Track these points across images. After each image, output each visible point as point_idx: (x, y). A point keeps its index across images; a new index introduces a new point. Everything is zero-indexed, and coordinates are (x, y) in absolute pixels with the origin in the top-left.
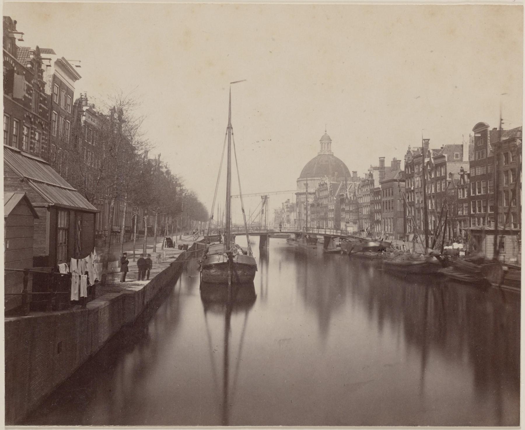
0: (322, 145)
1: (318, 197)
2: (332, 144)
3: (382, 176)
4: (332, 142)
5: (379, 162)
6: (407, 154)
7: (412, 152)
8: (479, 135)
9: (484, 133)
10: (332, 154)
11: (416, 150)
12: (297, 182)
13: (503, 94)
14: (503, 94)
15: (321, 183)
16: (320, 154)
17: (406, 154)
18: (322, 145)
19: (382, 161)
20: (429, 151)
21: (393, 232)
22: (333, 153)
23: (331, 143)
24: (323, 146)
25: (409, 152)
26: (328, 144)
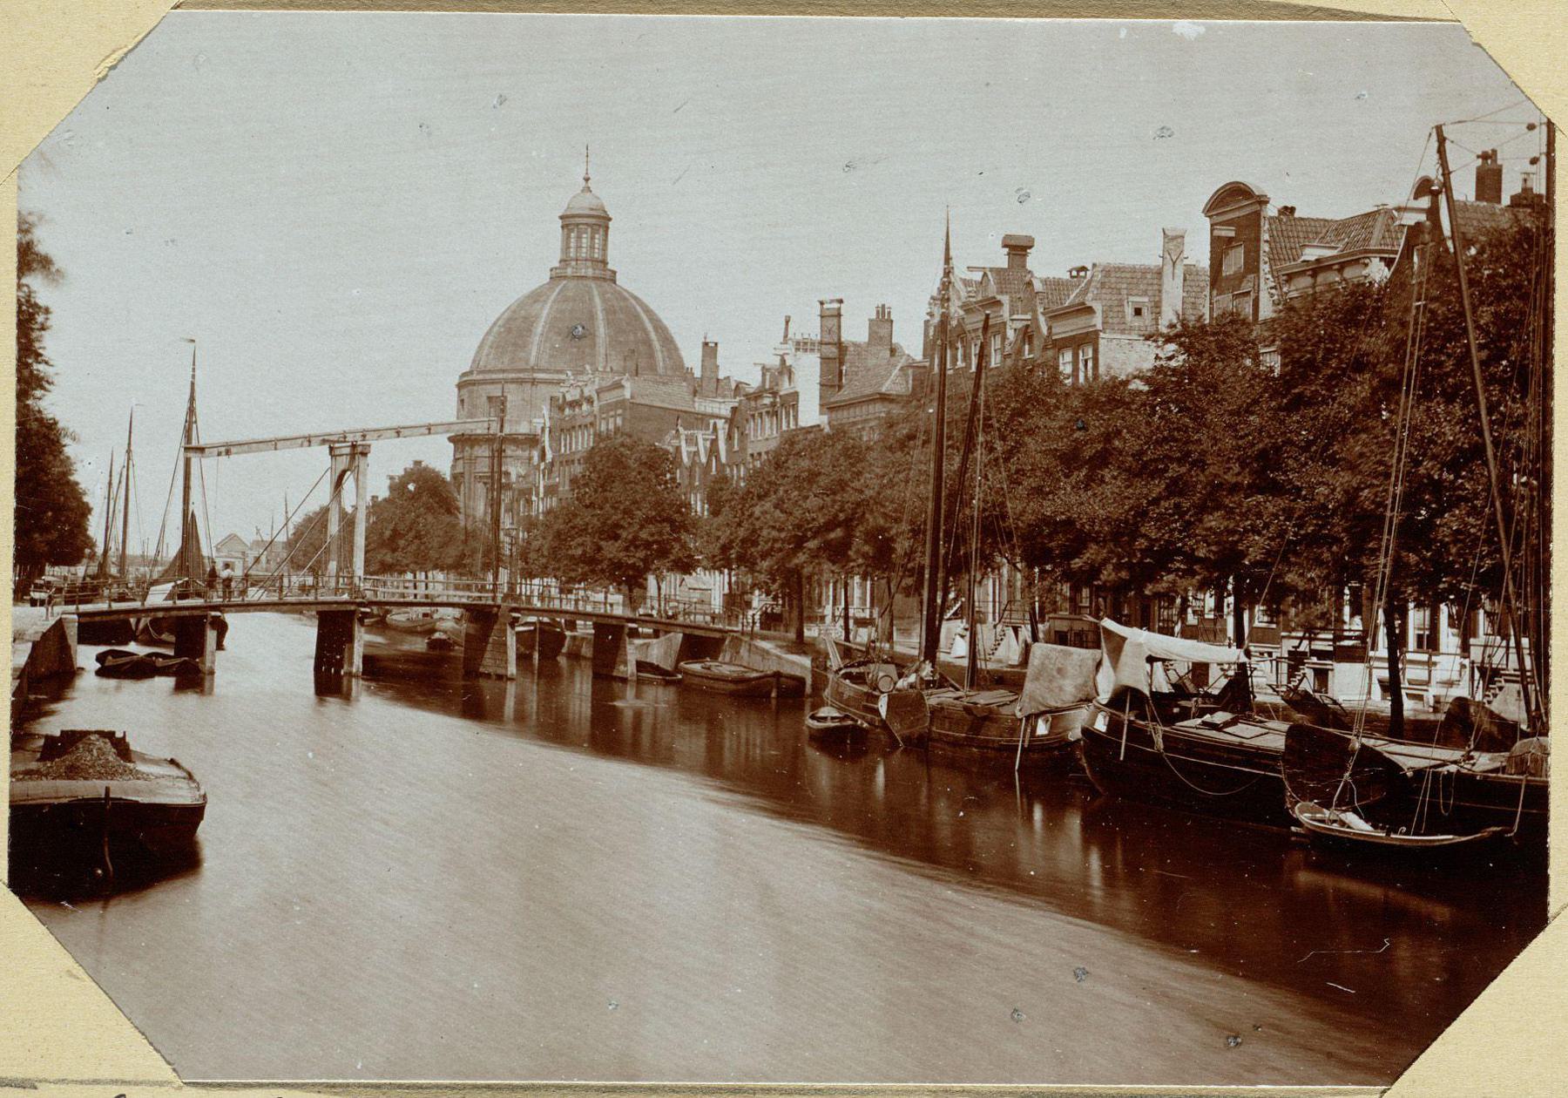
3: (833, 379)
12: (460, 386)
19: (831, 318)
22: (614, 273)
23: (607, 228)
26: (594, 233)
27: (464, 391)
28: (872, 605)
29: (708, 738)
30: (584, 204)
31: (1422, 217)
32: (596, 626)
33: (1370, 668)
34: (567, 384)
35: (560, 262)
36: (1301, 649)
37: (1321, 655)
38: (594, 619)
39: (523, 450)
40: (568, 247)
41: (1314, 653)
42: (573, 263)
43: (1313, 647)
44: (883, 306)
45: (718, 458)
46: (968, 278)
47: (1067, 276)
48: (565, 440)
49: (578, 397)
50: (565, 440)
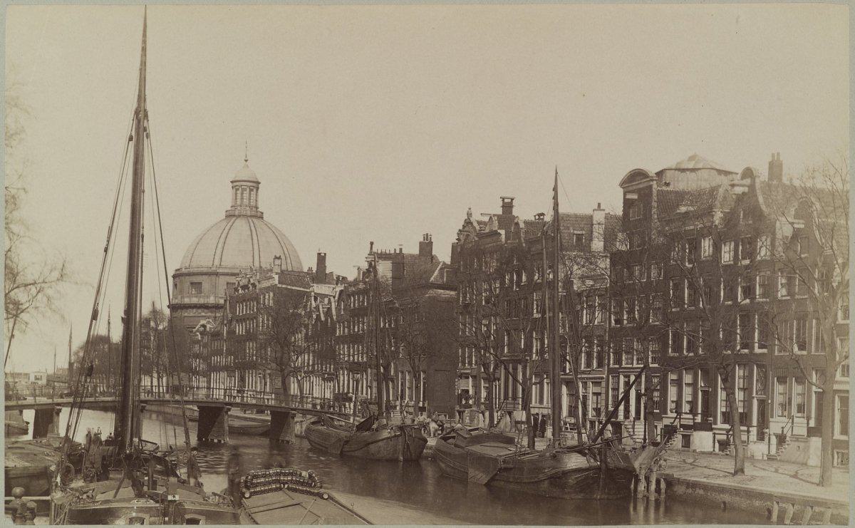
0: (236, 194)
1: (230, 316)
2: (260, 190)
4: (260, 185)
5: (4, 426)
6: (464, 226)
7: (475, 224)
8: (635, 197)
9: (645, 194)
10: (259, 214)
11: (486, 219)
13: (153, 303)
14: (153, 303)
15: (241, 284)
16: (232, 213)
17: (461, 228)
18: (236, 194)
20: (517, 224)
21: (424, 404)
22: (262, 213)
23: (258, 188)
24: (239, 195)
25: (468, 223)
27: (177, 279)
28: (424, 400)
29: (488, 481)
30: (244, 175)
31: (746, 189)
32: (272, 413)
33: (714, 434)
34: (240, 276)
35: (232, 207)
36: (675, 424)
37: (685, 427)
38: (36, 407)
39: (212, 312)
40: (236, 199)
41: (682, 426)
42: (239, 208)
43: (681, 423)
44: (427, 234)
45: (332, 319)
46: (480, 220)
47: (533, 219)
48: (239, 307)
49: (246, 283)
50: (239, 307)
